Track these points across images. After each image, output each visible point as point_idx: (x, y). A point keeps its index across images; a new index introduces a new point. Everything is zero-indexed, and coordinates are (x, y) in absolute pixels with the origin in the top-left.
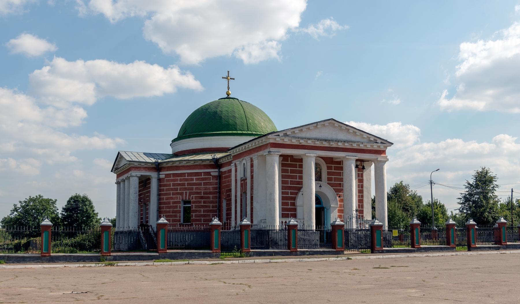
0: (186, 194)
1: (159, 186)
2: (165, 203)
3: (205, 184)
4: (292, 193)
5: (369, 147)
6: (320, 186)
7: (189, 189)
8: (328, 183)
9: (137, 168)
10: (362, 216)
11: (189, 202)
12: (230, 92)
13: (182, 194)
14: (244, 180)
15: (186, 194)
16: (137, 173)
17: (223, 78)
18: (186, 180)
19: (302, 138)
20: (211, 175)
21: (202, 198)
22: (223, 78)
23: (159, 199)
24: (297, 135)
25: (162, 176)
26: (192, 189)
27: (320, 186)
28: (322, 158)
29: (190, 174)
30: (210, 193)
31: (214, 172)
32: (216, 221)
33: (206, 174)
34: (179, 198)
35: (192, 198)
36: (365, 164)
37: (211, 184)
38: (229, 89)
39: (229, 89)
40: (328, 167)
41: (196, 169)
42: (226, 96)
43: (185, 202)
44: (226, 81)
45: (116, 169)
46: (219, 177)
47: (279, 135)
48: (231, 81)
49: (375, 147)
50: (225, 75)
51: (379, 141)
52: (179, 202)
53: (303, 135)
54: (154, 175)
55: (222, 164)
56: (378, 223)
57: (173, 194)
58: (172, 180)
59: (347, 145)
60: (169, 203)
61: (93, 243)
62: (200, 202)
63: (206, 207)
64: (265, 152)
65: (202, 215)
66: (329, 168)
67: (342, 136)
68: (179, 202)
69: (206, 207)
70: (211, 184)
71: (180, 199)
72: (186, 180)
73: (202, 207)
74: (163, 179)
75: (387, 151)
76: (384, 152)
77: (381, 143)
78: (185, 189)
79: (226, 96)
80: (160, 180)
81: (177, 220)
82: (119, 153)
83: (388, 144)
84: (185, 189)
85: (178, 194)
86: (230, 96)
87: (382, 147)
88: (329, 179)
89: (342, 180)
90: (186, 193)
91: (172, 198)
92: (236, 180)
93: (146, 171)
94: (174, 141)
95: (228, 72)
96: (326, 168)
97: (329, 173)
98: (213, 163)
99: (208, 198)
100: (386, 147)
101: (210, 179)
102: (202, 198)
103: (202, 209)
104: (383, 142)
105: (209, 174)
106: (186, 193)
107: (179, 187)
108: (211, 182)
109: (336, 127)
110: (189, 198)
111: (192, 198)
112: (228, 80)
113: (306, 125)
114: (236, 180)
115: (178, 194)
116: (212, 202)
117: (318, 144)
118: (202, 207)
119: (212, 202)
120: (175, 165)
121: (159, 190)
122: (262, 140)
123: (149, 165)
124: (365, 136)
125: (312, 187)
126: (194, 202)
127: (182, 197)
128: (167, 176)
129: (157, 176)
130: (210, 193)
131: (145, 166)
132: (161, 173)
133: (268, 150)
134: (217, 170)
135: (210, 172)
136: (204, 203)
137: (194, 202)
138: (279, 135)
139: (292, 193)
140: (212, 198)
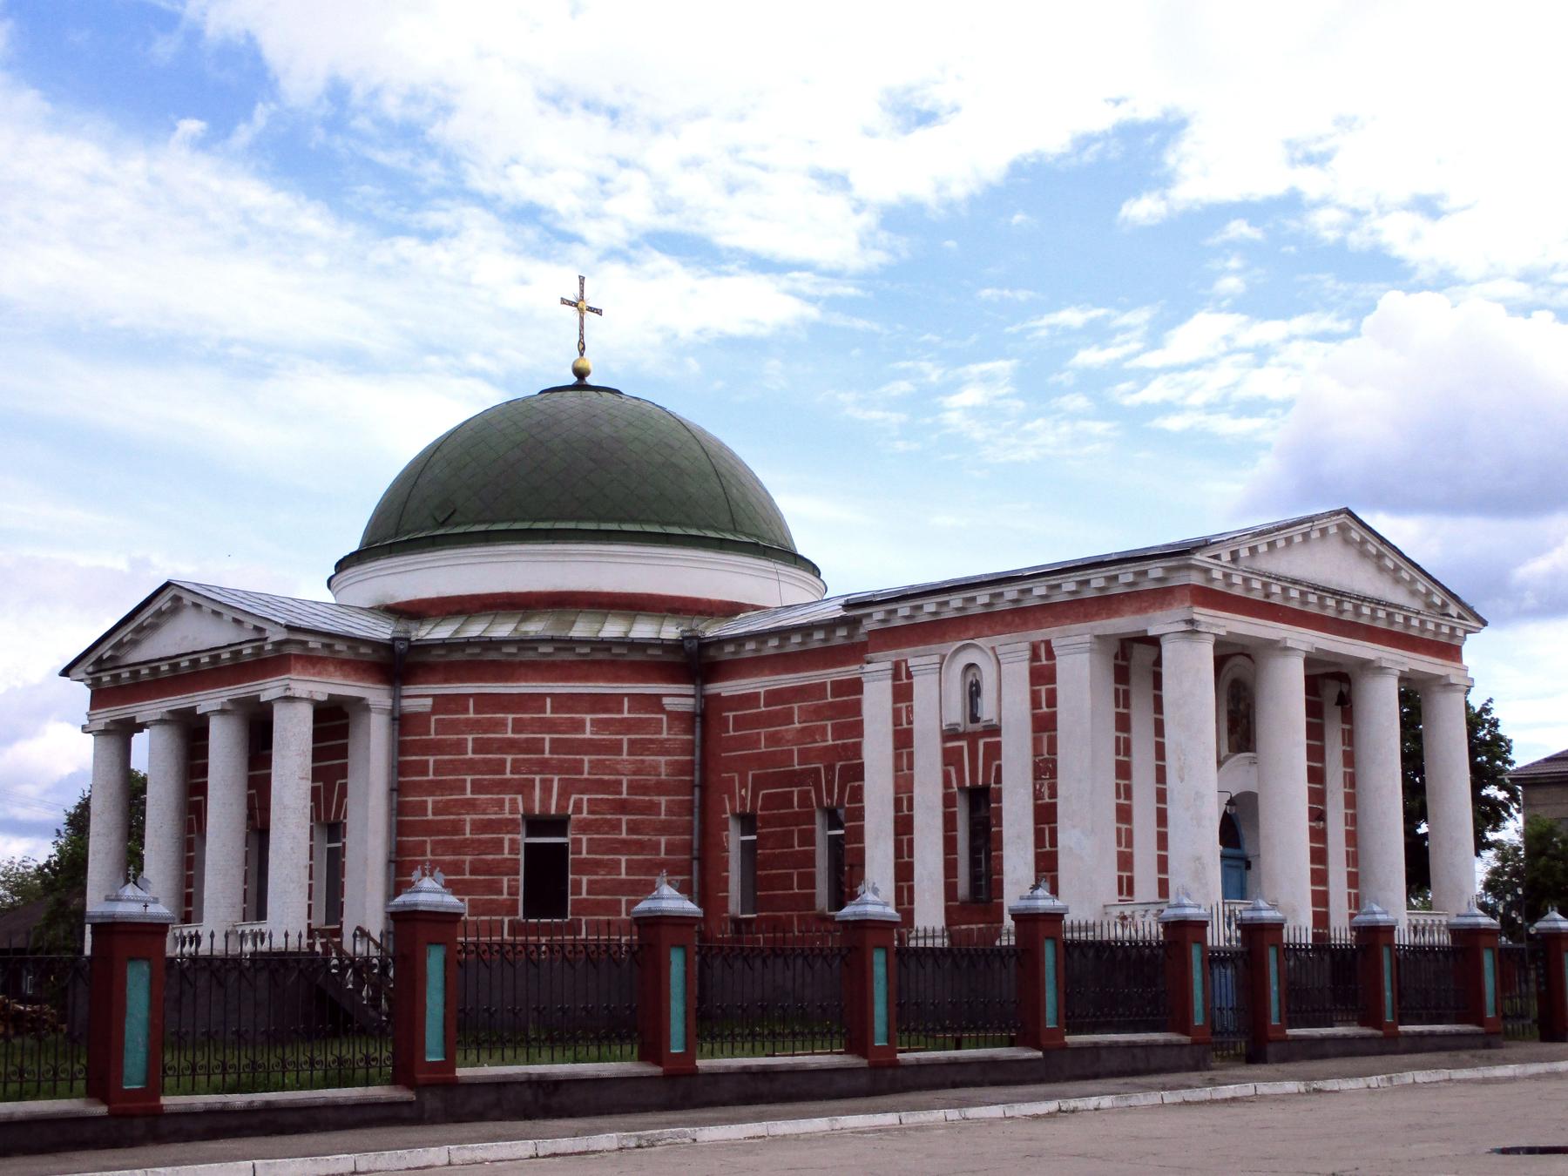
0: (546, 787)
2: (428, 828)
7: (560, 768)
9: (312, 662)
11: (558, 825)
13: (525, 788)
15: (546, 787)
18: (550, 726)
20: (662, 710)
21: (622, 807)
25: (411, 705)
26: (577, 767)
29: (561, 702)
30: (661, 788)
31: (678, 697)
33: (639, 701)
34: (512, 806)
35: (578, 809)
41: (586, 678)
42: (573, 380)
43: (536, 825)
45: (100, 664)
46: (706, 717)
48: (589, 316)
52: (509, 826)
54: (377, 696)
56: (436, 898)
57: (478, 787)
58: (473, 726)
60: (457, 828)
63: (641, 847)
65: (622, 882)
67: (1361, 579)
68: (509, 826)
69: (641, 847)
71: (514, 810)
72: (550, 726)
73: (625, 847)
75: (1464, 649)
78: (544, 766)
79: (573, 380)
80: (402, 722)
81: (501, 904)
84: (544, 766)
85: (504, 786)
86: (590, 380)
91: (471, 806)
92: (903, 739)
93: (346, 676)
102: (622, 807)
103: (623, 859)
104: (218, 608)
105: (654, 702)
107: (509, 758)
108: (662, 742)
109: (1354, 541)
110: (562, 805)
111: (578, 809)
112: (581, 311)
114: (903, 739)
115: (504, 786)
118: (625, 847)
119: (664, 828)
126: (585, 827)
127: (528, 800)
128: (442, 702)
129: (387, 703)
130: (661, 788)
134: (688, 689)
135: (659, 697)
136: (630, 830)
137: (585, 827)
140: (669, 811)
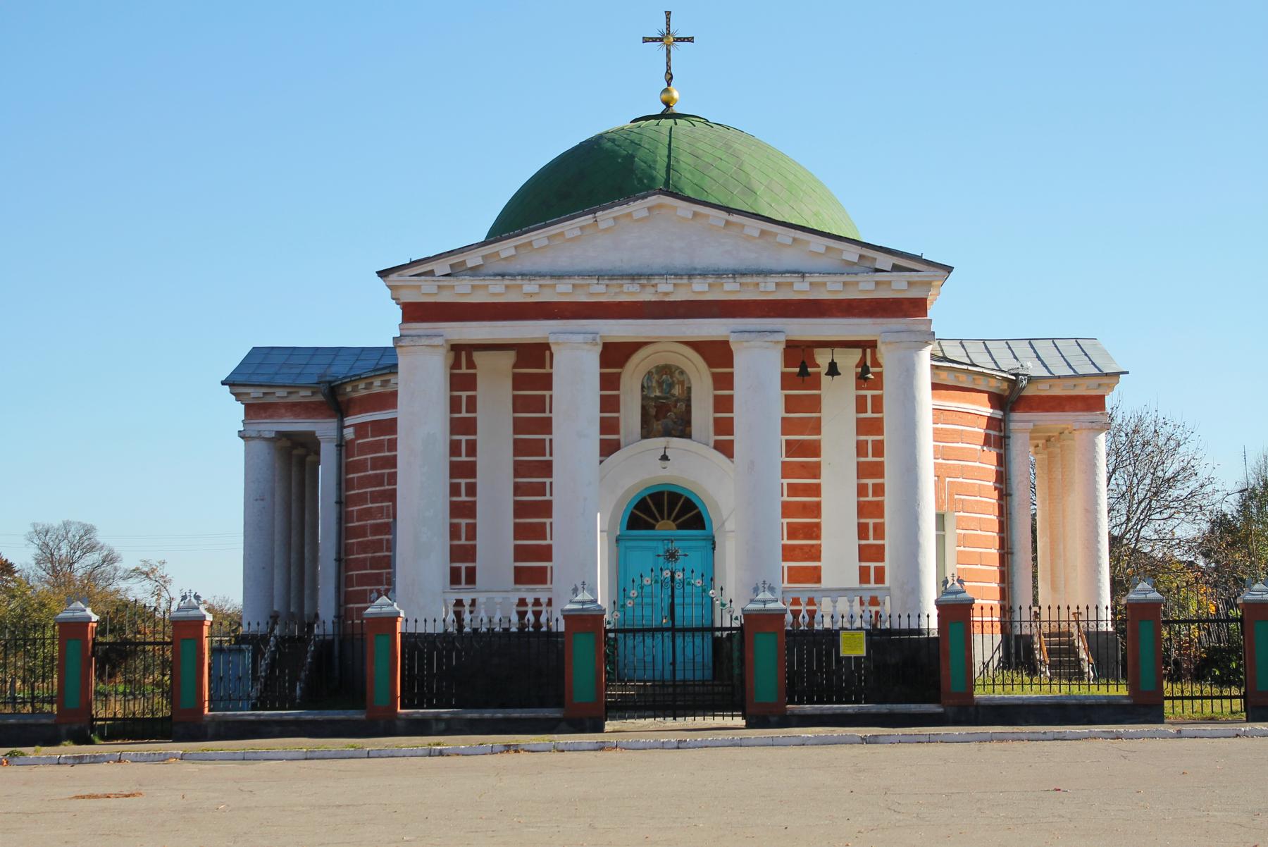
1: (344, 468)
5: (833, 289)
6: (665, 458)
12: (676, 94)
16: (262, 427)
17: (646, 40)
22: (646, 40)
24: (515, 267)
27: (665, 458)
28: (697, 346)
38: (669, 79)
39: (669, 79)
40: (714, 376)
44: (658, 50)
48: (679, 50)
54: (324, 429)
55: (351, 400)
61: (522, 627)
76: (917, 307)
77: (896, 268)
79: (659, 108)
80: (343, 446)
82: (949, 269)
83: (927, 273)
86: (677, 109)
87: (899, 287)
93: (297, 416)
95: (668, 14)
96: (709, 381)
98: (320, 398)
100: (928, 284)
113: (413, 264)
121: (342, 484)
122: (621, 286)
123: (303, 393)
124: (818, 244)
128: (360, 429)
132: (349, 421)
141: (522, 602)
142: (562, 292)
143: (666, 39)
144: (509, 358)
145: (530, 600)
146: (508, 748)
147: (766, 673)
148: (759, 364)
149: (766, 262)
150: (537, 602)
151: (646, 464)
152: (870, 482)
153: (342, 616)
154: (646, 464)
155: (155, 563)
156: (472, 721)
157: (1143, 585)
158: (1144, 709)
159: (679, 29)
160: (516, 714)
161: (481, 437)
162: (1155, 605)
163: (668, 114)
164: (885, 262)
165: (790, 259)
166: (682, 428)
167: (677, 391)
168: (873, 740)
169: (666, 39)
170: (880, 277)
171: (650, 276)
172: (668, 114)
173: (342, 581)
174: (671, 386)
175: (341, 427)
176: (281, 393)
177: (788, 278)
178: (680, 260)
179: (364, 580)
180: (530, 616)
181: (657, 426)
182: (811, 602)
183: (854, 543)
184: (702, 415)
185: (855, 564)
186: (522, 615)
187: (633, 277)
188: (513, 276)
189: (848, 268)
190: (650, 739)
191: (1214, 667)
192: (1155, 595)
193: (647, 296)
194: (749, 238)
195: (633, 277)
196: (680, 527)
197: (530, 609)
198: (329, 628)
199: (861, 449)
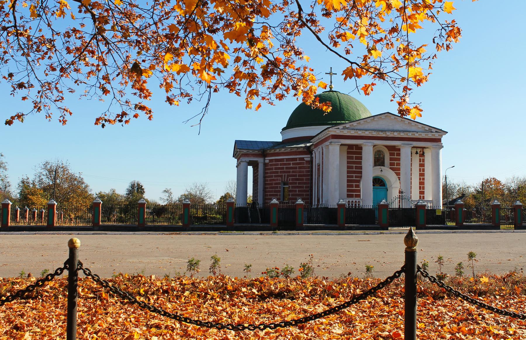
1: (265, 169)
3: (300, 168)
4: (356, 177)
5: (423, 136)
6: (381, 171)
8: (391, 168)
10: (424, 197)
13: (281, 176)
14: (319, 166)
19: (360, 130)
21: (297, 179)
23: (265, 180)
24: (356, 128)
25: (267, 161)
27: (381, 171)
28: (386, 146)
29: (288, 160)
31: (307, 157)
32: (300, 201)
36: (425, 150)
37: (304, 168)
44: (329, 76)
47: (338, 128)
48: (333, 76)
49: (430, 136)
50: (329, 71)
51: (434, 130)
52: (279, 184)
53: (366, 127)
54: (260, 160)
57: (275, 176)
59: (402, 135)
61: (349, 207)
62: (296, 183)
64: (327, 143)
66: (391, 154)
68: (279, 184)
70: (304, 168)
74: (268, 163)
75: (442, 139)
76: (439, 140)
77: (436, 132)
78: (284, 172)
80: (265, 165)
84: (284, 172)
86: (333, 89)
87: (437, 136)
88: (391, 164)
89: (361, 168)
90: (285, 175)
94: (284, 129)
96: (389, 154)
97: (391, 159)
98: (260, 153)
99: (302, 180)
100: (442, 136)
101: (303, 163)
105: (303, 159)
106: (285, 175)
116: (305, 183)
117: (375, 134)
120: (293, 150)
121: (265, 173)
124: (420, 126)
125: (369, 171)
126: (291, 183)
130: (304, 176)
131: (254, 153)
132: (266, 158)
133: (330, 141)
137: (291, 183)
138: (338, 128)
139: (356, 177)
141: (349, 202)
142: (367, 134)
143: (331, 74)
144: (346, 147)
145: (351, 201)
146: (381, 233)
147: (422, 219)
148: (406, 150)
149: (409, 129)
150: (356, 202)
151: (377, 172)
152: (422, 177)
153: (264, 203)
154: (377, 172)
155: (169, 189)
156: (361, 227)
157: (274, 200)
158: (496, 227)
159: (333, 72)
160: (371, 226)
161: (426, 168)
162: (499, 205)
163: (331, 91)
164: (434, 130)
165: (414, 129)
166: (383, 164)
167: (381, 156)
168: (455, 232)
169: (331, 74)
170: (433, 133)
171: (385, 131)
172: (331, 91)
173: (265, 195)
174: (380, 155)
175: (265, 160)
176: (251, 151)
177: (414, 133)
178: (391, 128)
179: (270, 195)
180: (357, 205)
181: (377, 164)
182: (359, 202)
183: (418, 191)
184: (387, 161)
185: (419, 195)
186: (349, 204)
187: (382, 131)
188: (357, 130)
189: (426, 131)
190: (397, 232)
191: (507, 220)
192: (499, 203)
193: (384, 135)
194: (405, 124)
195: (382, 131)
196: (380, 186)
197: (357, 203)
198: (262, 206)
199: (420, 170)
